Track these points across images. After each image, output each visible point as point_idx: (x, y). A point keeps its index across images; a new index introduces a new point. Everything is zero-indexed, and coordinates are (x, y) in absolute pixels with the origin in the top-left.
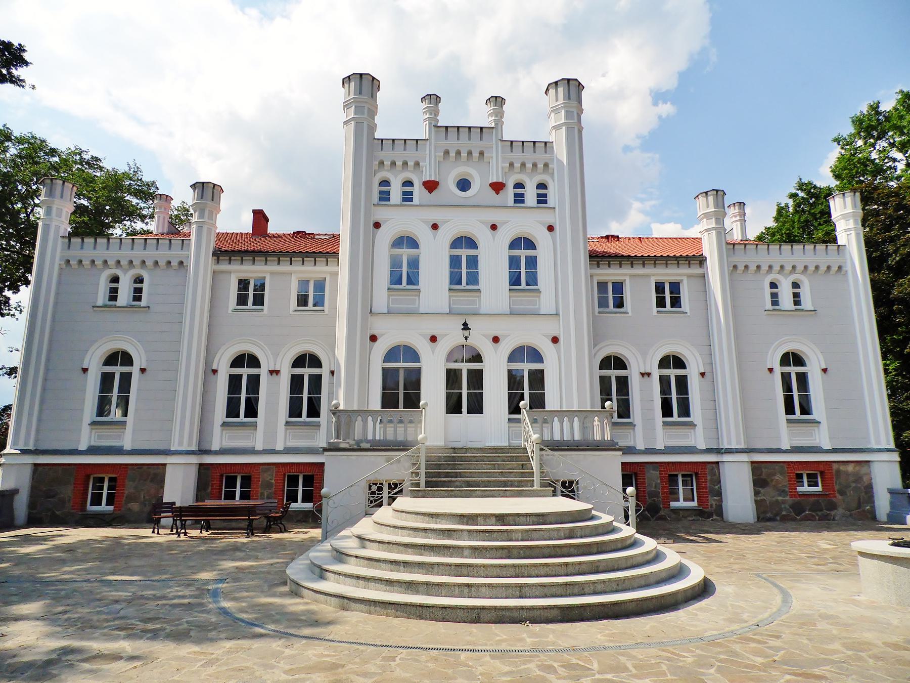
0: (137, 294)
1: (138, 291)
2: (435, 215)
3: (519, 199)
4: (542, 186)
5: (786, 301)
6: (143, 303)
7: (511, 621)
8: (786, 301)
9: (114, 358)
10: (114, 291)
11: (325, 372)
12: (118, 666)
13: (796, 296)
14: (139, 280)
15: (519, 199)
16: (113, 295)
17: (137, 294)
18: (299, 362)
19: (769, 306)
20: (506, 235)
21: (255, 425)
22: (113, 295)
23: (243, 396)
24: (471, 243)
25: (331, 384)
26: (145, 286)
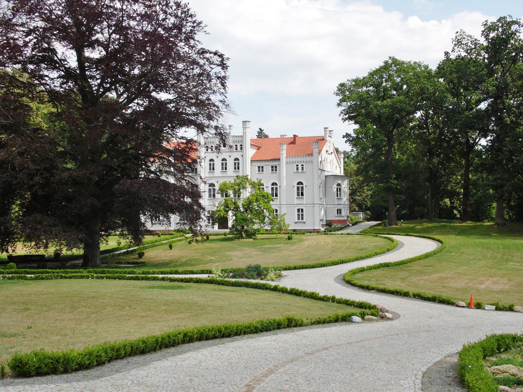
0: (303, 169)
1: (303, 168)
2: (230, 154)
3: (236, 148)
4: (241, 145)
5: (300, 167)
6: (304, 171)
7: (54, 267)
8: (300, 167)
9: (299, 183)
10: (298, 168)
11: (278, 186)
12: (131, 270)
13: (303, 168)
14: (302, 165)
15: (236, 148)
16: (297, 169)
17: (303, 169)
18: (273, 184)
19: (295, 171)
20: (233, 158)
21: (303, 198)
22: (297, 169)
23: (300, 191)
24: (225, 160)
25: (280, 190)
26: (304, 167)
